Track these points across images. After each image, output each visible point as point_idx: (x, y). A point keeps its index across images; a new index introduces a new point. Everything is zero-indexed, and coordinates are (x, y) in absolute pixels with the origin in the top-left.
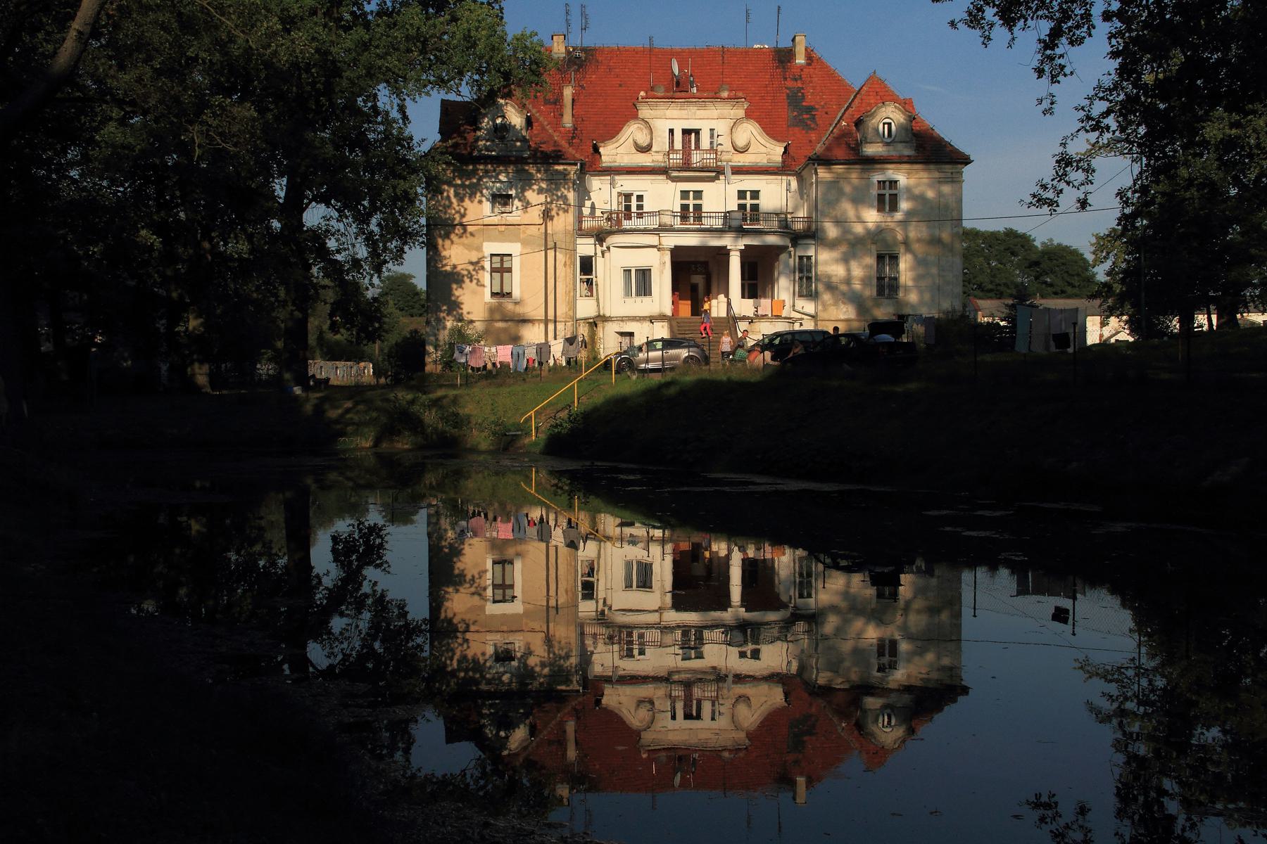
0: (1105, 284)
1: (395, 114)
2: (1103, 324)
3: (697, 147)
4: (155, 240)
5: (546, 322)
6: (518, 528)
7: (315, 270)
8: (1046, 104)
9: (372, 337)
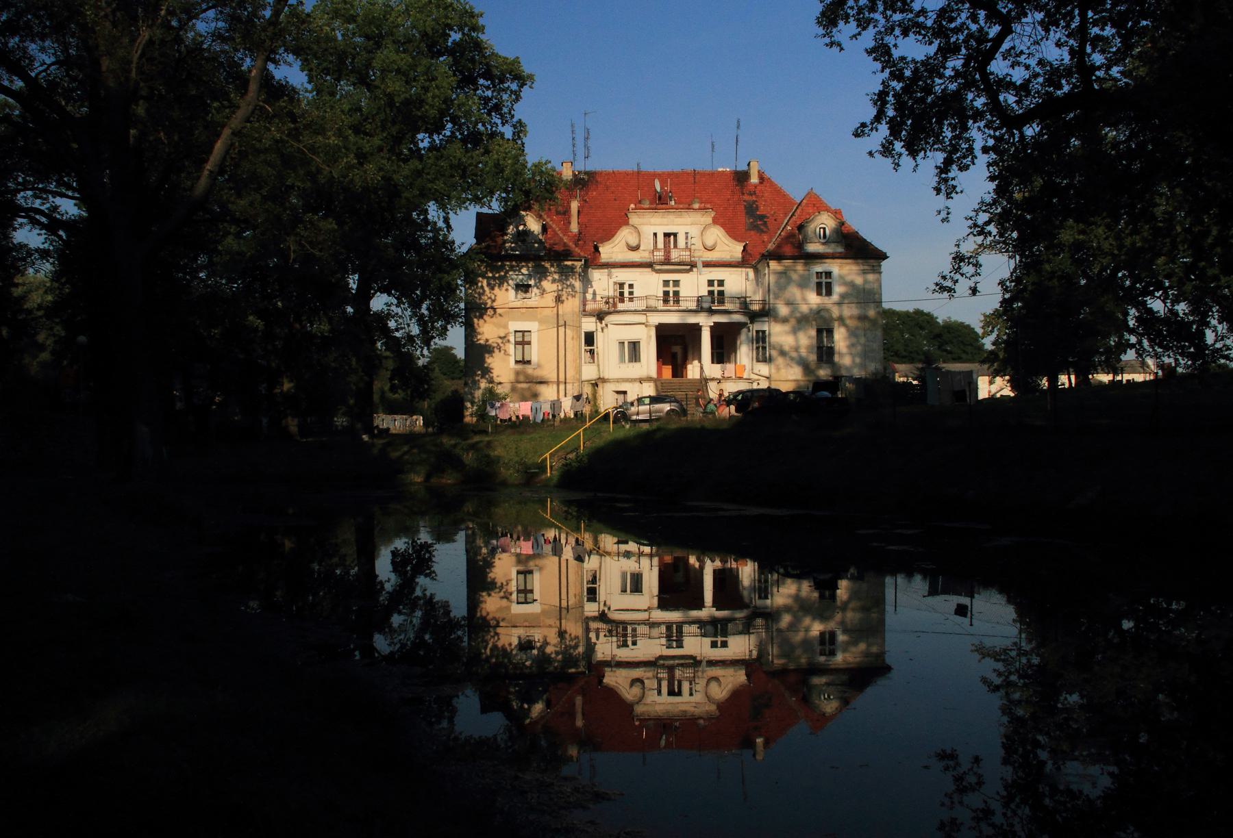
0: (992, 352)
1: (441, 224)
2: (991, 383)
3: (675, 246)
4: (259, 323)
5: (558, 383)
6: (536, 545)
7: (379, 344)
8: (943, 215)
9: (423, 395)
